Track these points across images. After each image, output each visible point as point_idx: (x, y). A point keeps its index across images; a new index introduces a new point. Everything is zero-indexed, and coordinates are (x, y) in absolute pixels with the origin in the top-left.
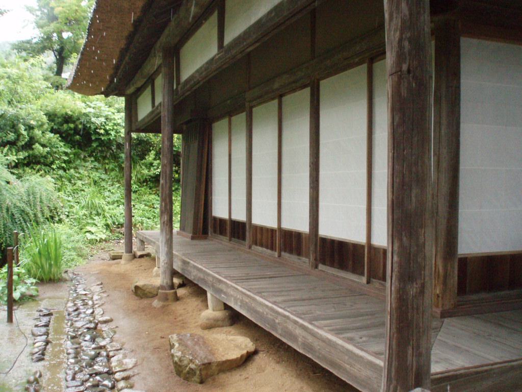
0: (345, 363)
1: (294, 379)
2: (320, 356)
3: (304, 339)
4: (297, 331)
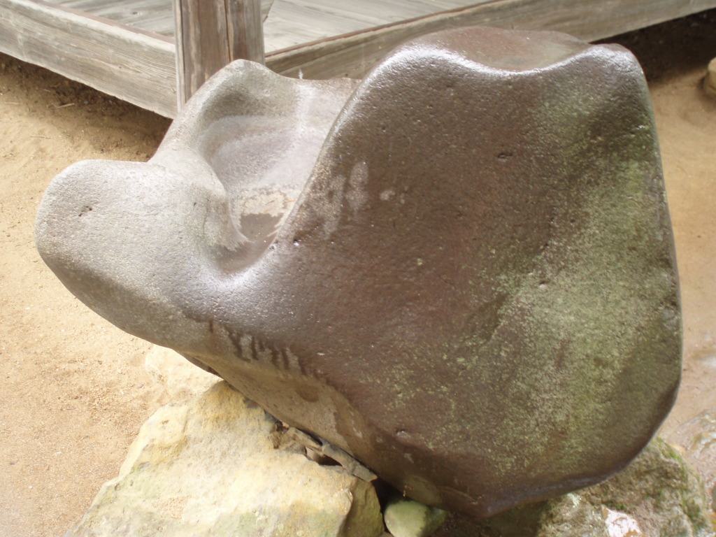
0: (109, 63)
1: (24, 120)
2: (63, 59)
3: (27, 34)
4: (11, 22)
